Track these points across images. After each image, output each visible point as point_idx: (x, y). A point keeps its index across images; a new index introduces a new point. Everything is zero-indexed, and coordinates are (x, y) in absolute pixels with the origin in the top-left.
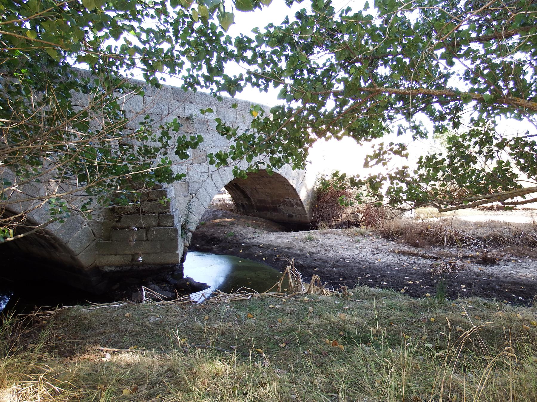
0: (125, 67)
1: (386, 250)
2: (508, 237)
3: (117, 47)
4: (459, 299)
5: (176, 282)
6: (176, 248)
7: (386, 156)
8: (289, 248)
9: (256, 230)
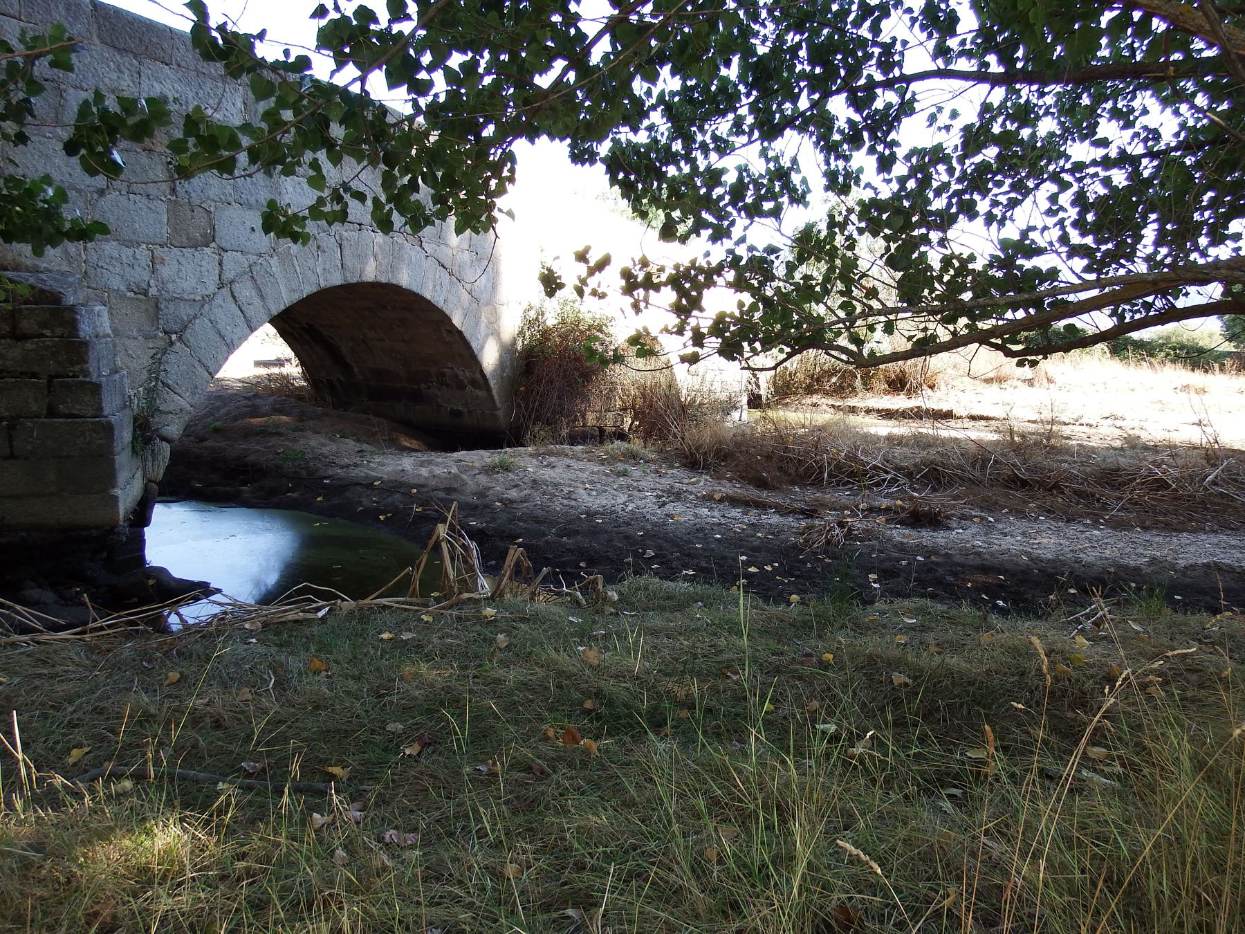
1: (691, 493)
2: (960, 467)
9: (365, 447)
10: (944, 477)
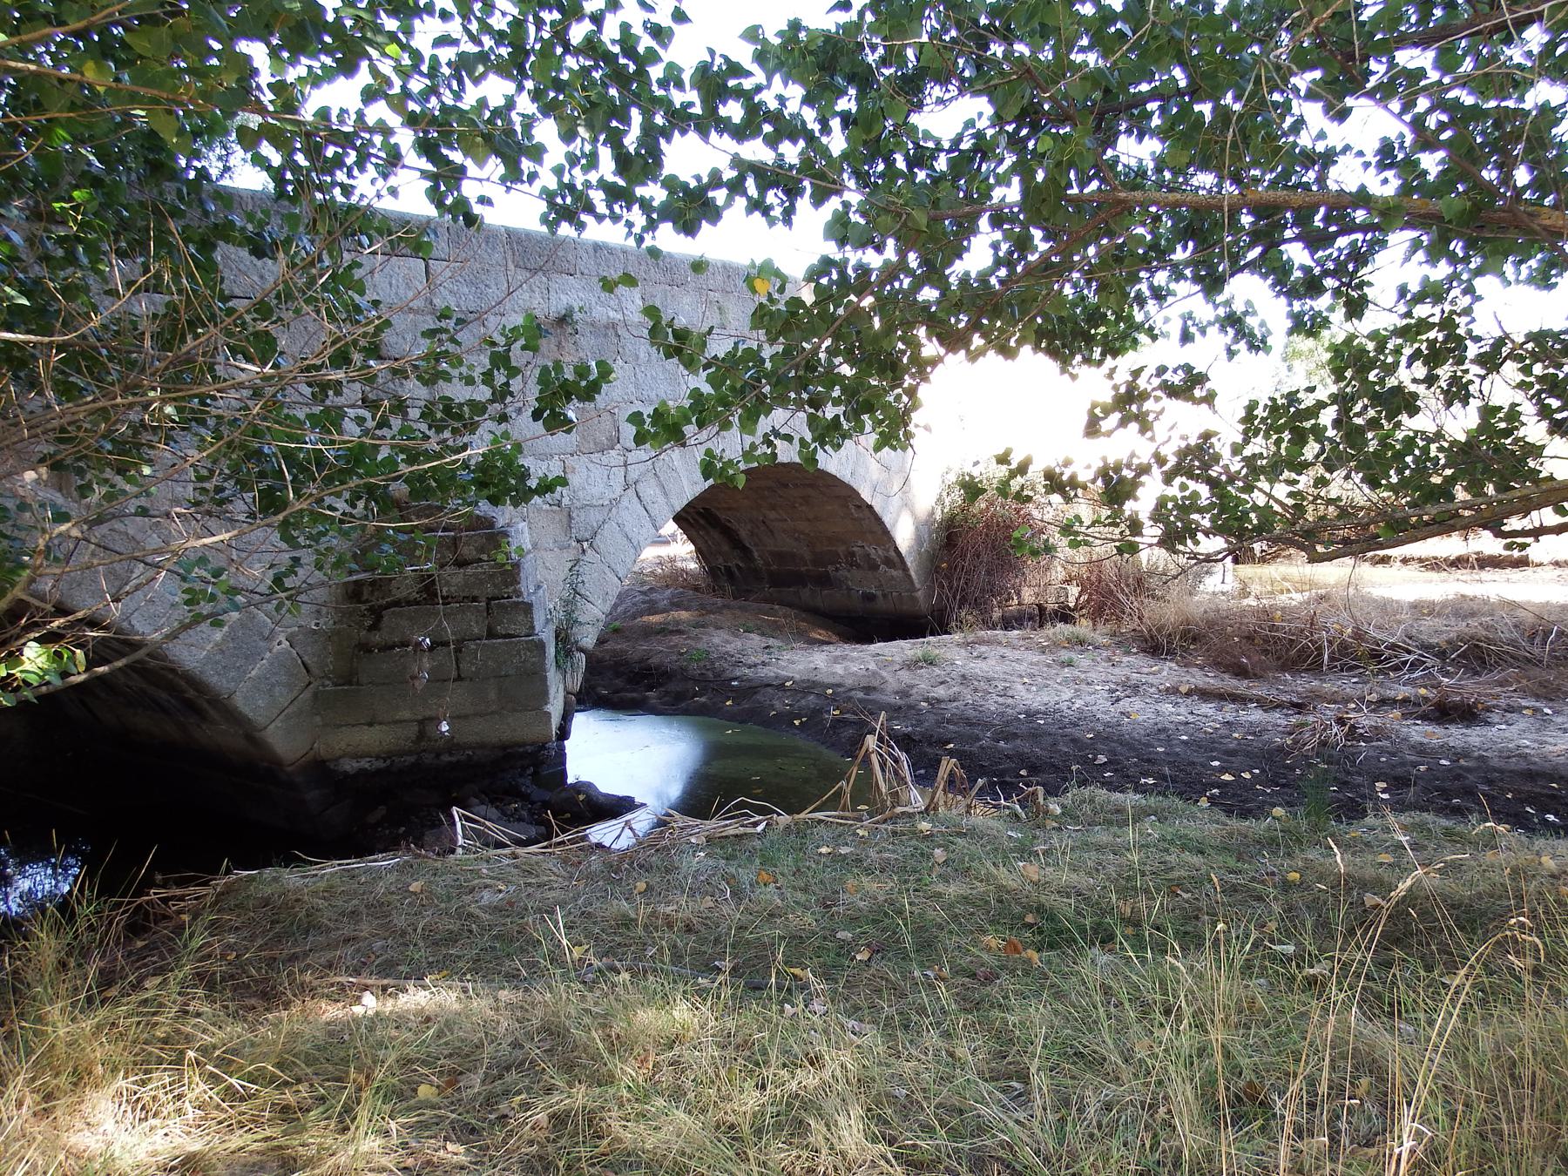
0: (371, 171)
1: (1152, 685)
2: (1512, 643)
3: (346, 111)
4: (1370, 820)
5: (547, 796)
6: (543, 696)
7: (1149, 405)
8: (868, 689)
9: (771, 641)
10: (1489, 655)
